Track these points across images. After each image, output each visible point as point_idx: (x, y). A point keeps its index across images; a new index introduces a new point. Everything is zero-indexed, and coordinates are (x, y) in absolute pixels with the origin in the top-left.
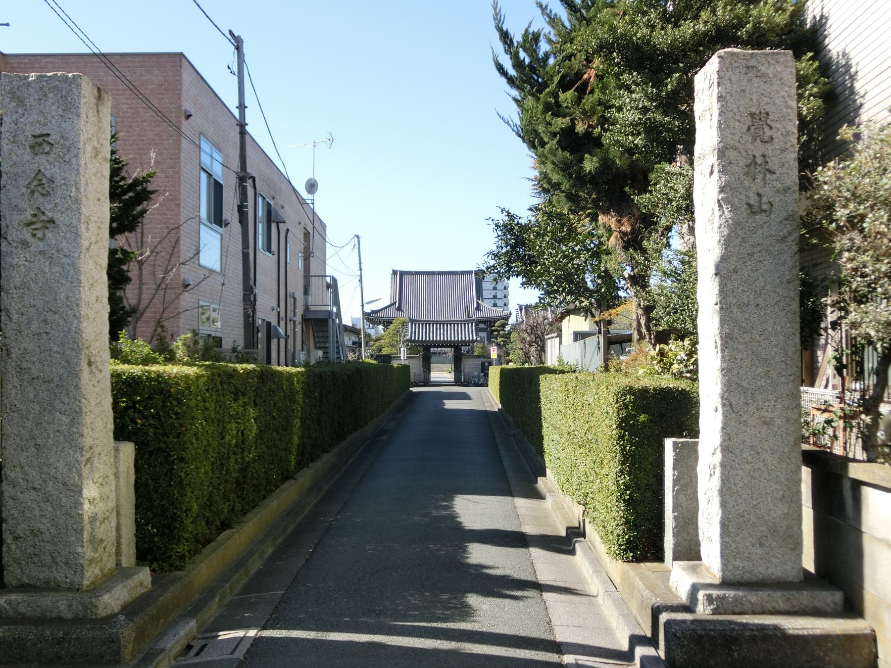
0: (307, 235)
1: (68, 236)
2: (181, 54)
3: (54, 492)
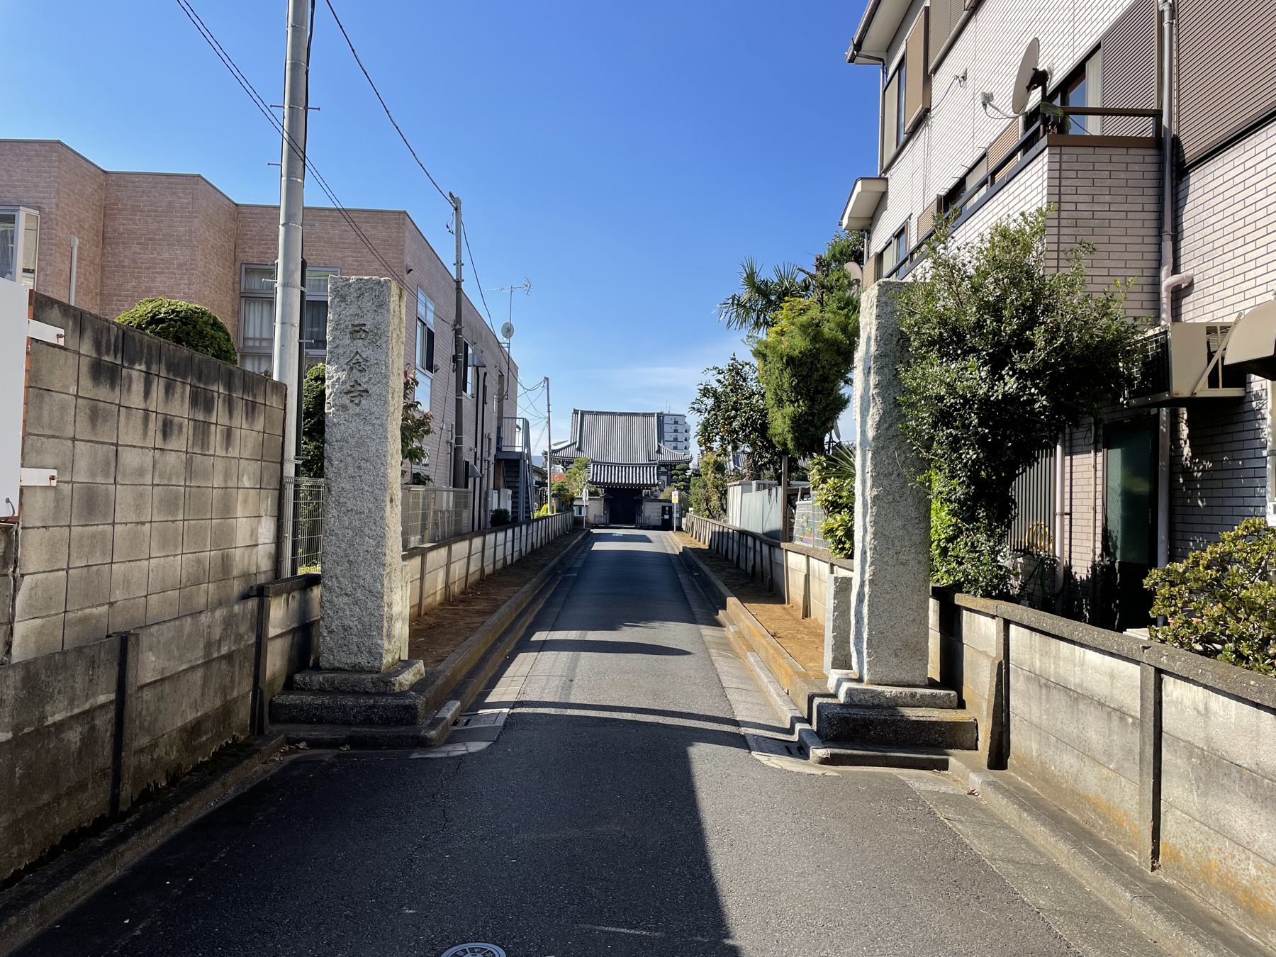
0: (501, 376)
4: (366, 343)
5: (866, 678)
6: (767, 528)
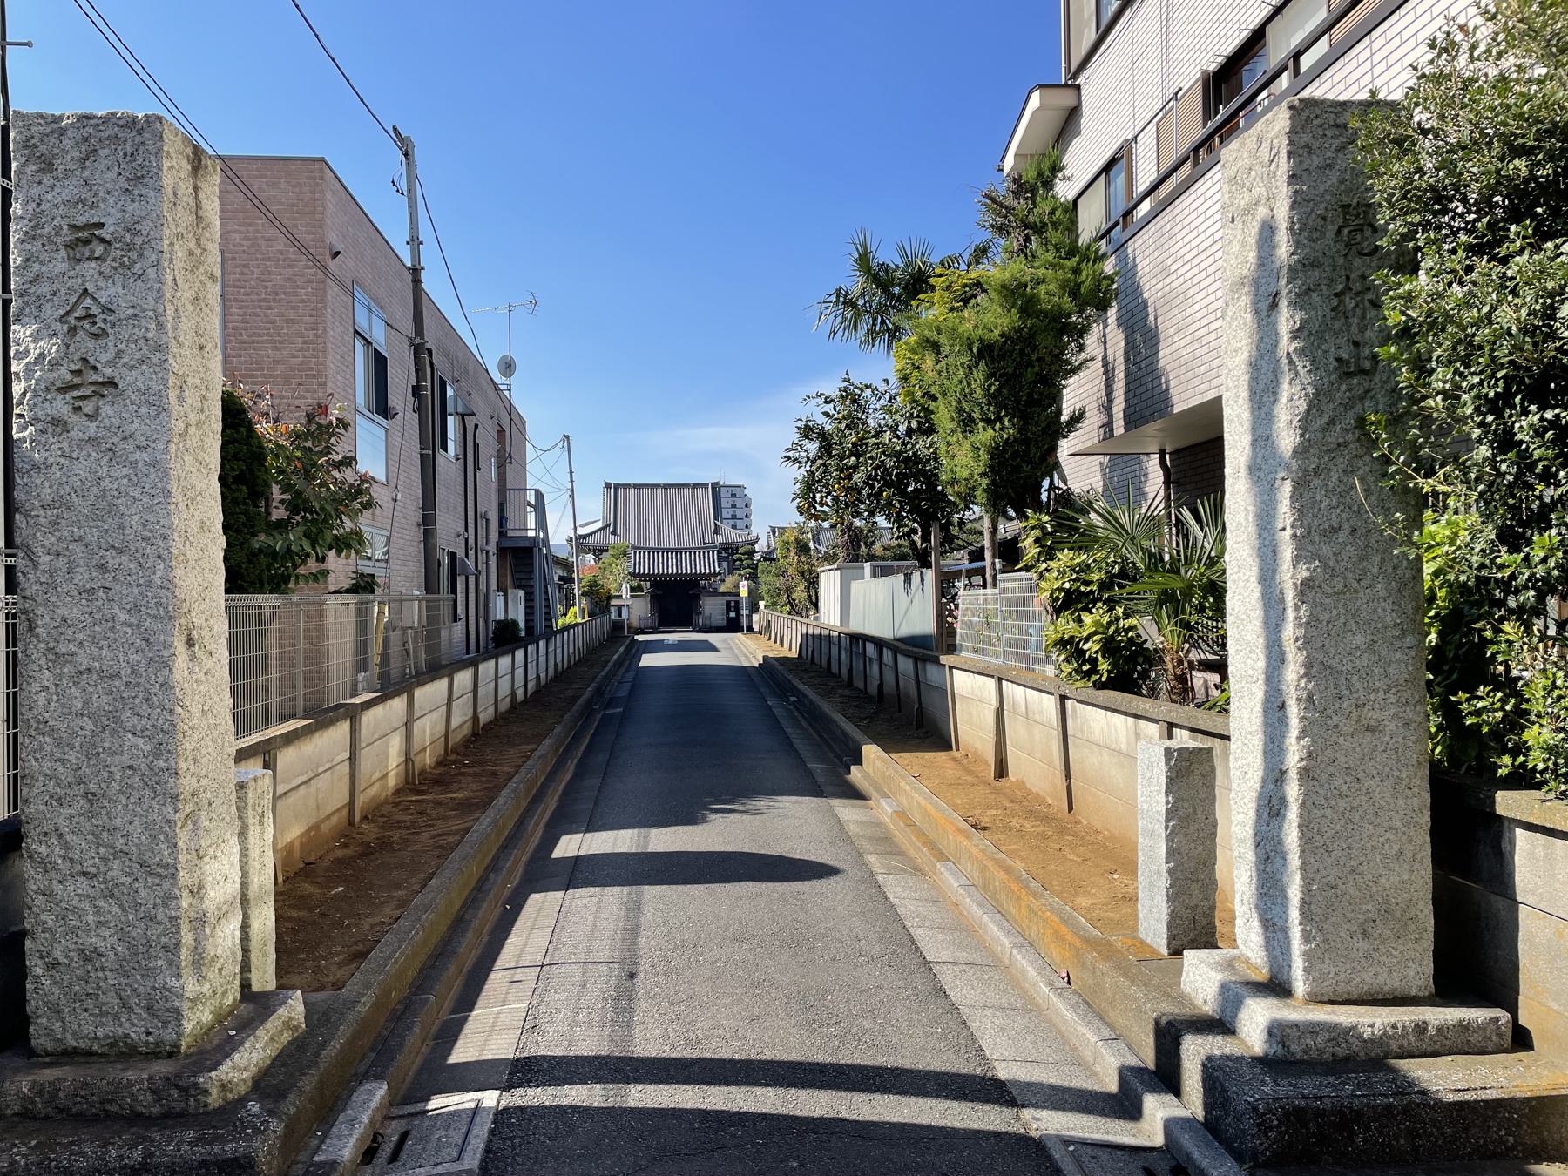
0: (501, 433)
1: (143, 411)
2: (323, 160)
3: (123, 880)
4: (106, 267)
5: (1300, 987)
6: (905, 631)
